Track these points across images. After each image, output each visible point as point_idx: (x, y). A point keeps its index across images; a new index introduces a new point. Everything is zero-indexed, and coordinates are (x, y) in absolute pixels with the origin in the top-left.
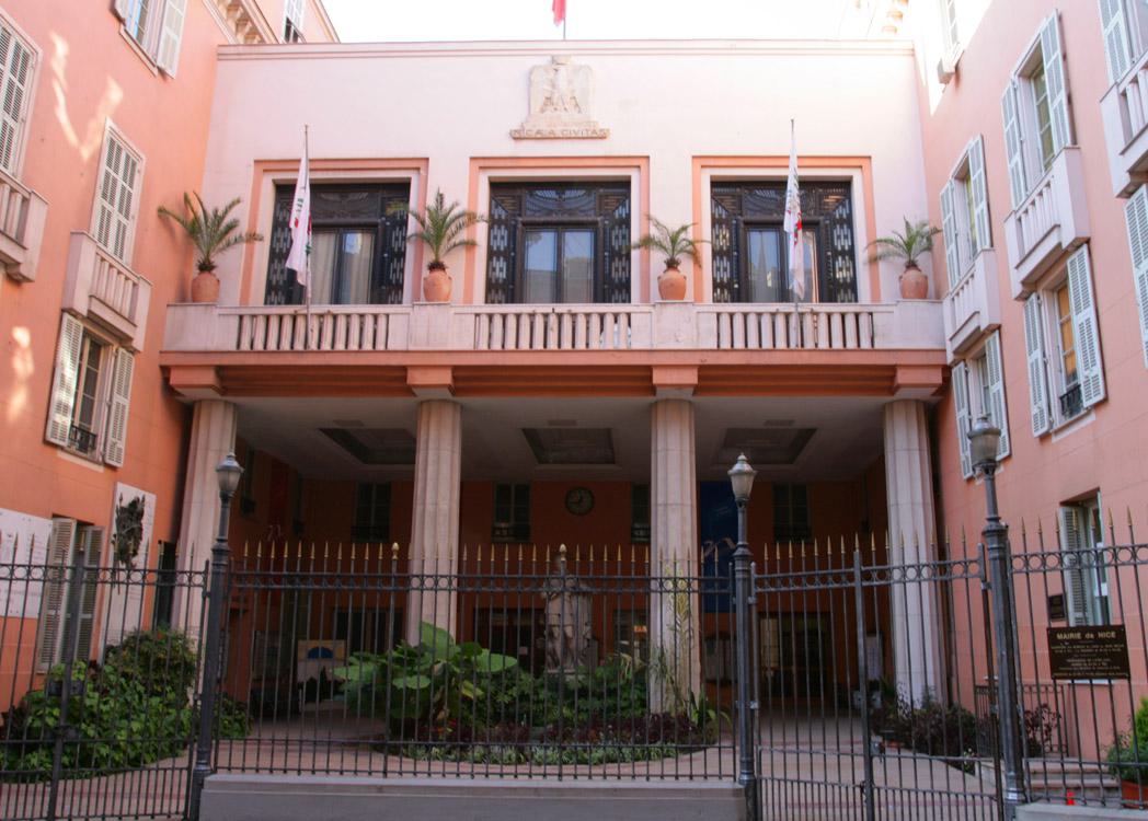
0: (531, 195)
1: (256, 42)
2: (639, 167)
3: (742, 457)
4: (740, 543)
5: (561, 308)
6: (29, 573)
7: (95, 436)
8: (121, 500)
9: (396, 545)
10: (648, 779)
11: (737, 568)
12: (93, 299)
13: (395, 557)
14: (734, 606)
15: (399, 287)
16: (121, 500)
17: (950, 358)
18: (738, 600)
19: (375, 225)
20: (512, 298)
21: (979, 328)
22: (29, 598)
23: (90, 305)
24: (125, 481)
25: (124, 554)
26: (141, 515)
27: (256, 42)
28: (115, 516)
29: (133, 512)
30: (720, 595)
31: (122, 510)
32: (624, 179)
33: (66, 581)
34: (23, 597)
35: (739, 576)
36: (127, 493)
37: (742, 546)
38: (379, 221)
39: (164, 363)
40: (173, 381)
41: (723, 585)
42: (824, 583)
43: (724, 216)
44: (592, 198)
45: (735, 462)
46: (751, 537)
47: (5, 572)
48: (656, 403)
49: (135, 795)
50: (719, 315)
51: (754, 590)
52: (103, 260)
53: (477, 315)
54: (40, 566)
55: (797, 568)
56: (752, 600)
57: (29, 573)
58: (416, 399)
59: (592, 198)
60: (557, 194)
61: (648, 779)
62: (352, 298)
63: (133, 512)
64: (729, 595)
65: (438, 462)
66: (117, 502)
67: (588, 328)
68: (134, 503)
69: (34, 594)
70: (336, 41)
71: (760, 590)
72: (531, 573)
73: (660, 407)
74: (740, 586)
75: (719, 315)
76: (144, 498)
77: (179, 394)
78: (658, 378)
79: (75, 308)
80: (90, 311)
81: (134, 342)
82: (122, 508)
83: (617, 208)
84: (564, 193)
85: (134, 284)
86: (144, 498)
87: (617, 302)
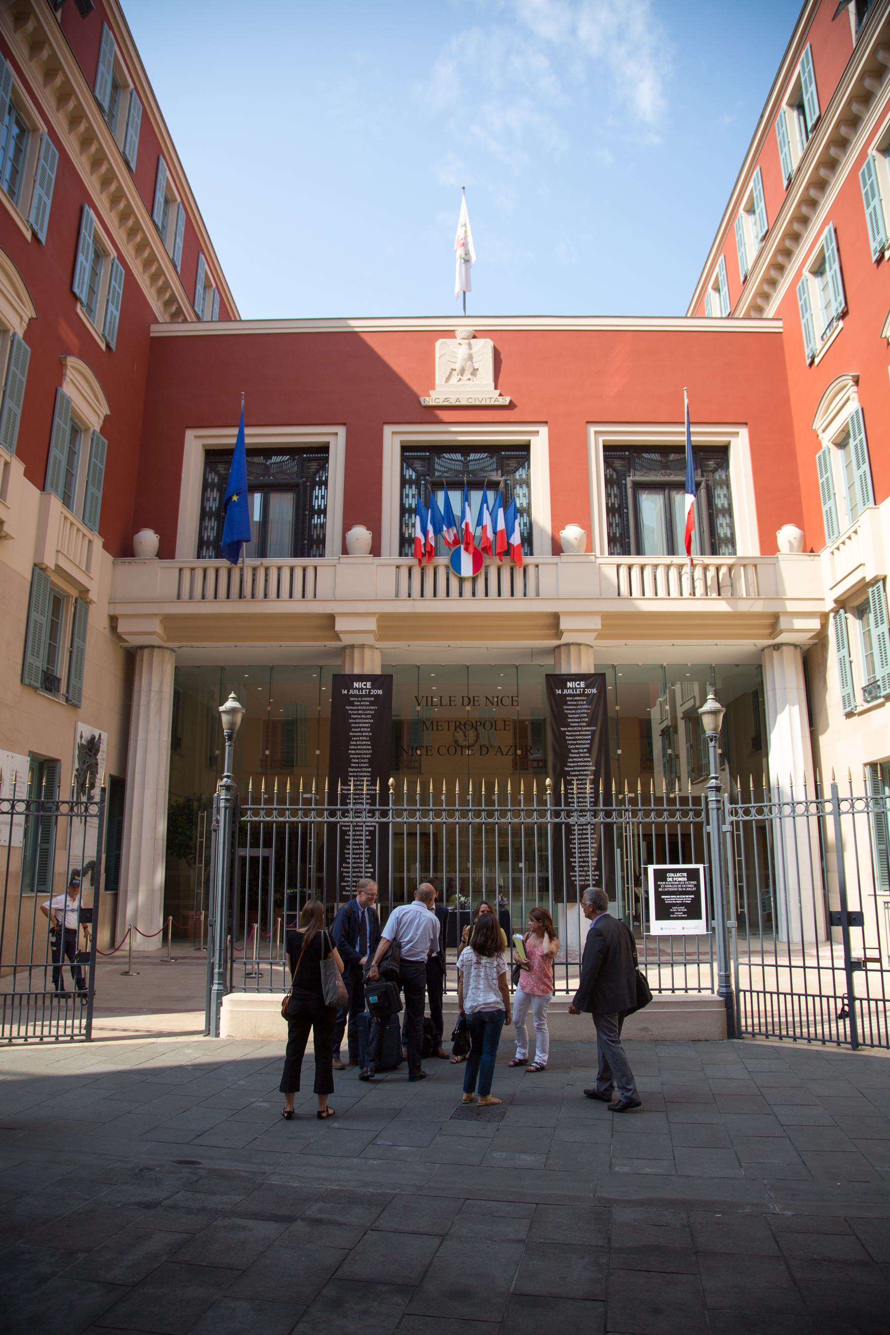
0: (439, 458)
1: (180, 320)
2: (336, 434)
3: (232, 695)
4: (225, 774)
5: (267, 561)
6: (13, 807)
7: (60, 680)
8: (81, 737)
9: (391, 780)
10: (699, 991)
11: (710, 799)
12: (60, 554)
13: (391, 791)
14: (708, 834)
15: (321, 542)
16: (81, 737)
17: (829, 605)
18: (711, 828)
19: (297, 486)
20: (626, 552)
21: (864, 578)
22: (14, 828)
23: (57, 558)
24: (86, 722)
25: (83, 785)
26: (97, 751)
27: (180, 320)
28: (77, 752)
29: (90, 748)
30: (329, 823)
31: (81, 747)
32: (681, 444)
33: (830, 814)
34: (9, 827)
35: (712, 805)
36: (86, 731)
37: (228, 777)
38: (501, 479)
39: (112, 613)
40: (120, 629)
41: (697, 814)
42: (759, 815)
43: (414, 477)
44: (494, 459)
45: (226, 700)
46: (235, 769)
47: (6, 807)
48: (559, 647)
49: (749, 1014)
50: (618, 566)
51: (729, 819)
52: (66, 518)
53: (398, 567)
54: (23, 801)
55: (746, 800)
56: (727, 828)
57: (13, 807)
58: (340, 643)
59: (494, 459)
60: (462, 456)
61: (699, 991)
62: (268, 555)
63: (90, 748)
64: (702, 823)
65: (149, 702)
66: (78, 740)
67: (266, 580)
68: (93, 738)
69: (19, 825)
70: (238, 319)
71: (734, 818)
72: (676, 805)
73: (563, 648)
74: (713, 815)
75: (618, 566)
76: (100, 736)
77: (126, 641)
78: (340, 625)
79: (111, 558)
80: (57, 566)
81: (90, 593)
82: (82, 744)
83: (517, 470)
84: (469, 456)
85: (90, 542)
86: (100, 736)
87: (315, 556)
